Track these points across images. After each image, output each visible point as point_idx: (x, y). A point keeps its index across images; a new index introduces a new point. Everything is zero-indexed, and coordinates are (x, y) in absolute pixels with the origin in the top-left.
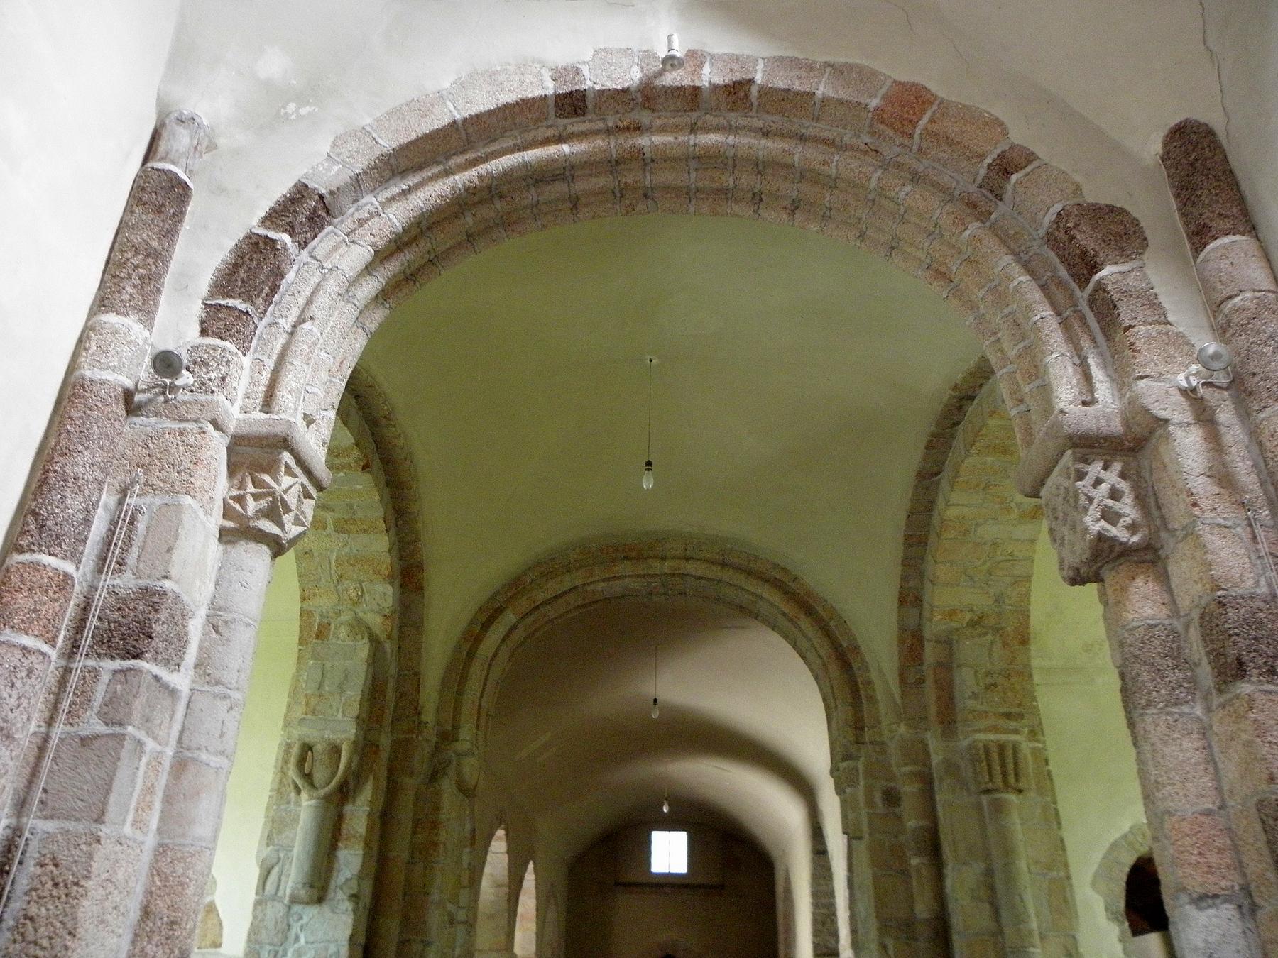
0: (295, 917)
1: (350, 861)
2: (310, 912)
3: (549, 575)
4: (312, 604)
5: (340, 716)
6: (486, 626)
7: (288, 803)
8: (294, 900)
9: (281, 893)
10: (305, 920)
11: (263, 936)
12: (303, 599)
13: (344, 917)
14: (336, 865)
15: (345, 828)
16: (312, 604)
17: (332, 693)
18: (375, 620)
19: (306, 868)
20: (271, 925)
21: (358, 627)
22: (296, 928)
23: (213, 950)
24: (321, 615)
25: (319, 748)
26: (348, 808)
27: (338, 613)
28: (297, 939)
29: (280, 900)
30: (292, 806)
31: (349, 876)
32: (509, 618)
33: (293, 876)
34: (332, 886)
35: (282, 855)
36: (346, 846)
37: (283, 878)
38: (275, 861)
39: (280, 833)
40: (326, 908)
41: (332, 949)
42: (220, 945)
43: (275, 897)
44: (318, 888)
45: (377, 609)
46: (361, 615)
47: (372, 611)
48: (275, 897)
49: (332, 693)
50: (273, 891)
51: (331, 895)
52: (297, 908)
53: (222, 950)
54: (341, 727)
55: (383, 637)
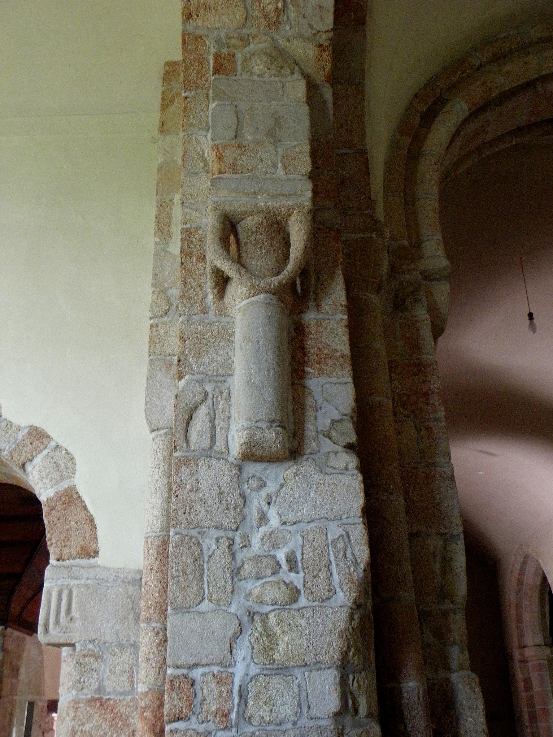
0: (254, 484)
1: (332, 395)
2: (279, 476)
3: (500, 58)
4: (197, 25)
5: (280, 172)
6: (429, 117)
7: (205, 311)
8: (252, 454)
9: (219, 446)
10: (271, 487)
11: (201, 515)
12: (188, 16)
13: (345, 479)
14: (309, 401)
15: (311, 344)
16: (197, 25)
17: (259, 143)
18: (306, 52)
19: (269, 395)
20: (212, 496)
21: (280, 58)
22: (257, 502)
23: (83, 562)
24: (218, 42)
25: (249, 222)
26: (310, 317)
27: (245, 41)
28: (263, 518)
29: (222, 456)
30: (212, 316)
31: (336, 415)
32: (458, 109)
33: (243, 410)
34: (310, 430)
35: (209, 388)
36: (321, 372)
37: (219, 425)
38: (199, 397)
39: (198, 354)
40: (307, 467)
41: (335, 531)
42: (96, 553)
43: (210, 451)
44: (289, 437)
45: (308, 33)
46: (281, 42)
47: (301, 36)
48: (210, 451)
49: (259, 143)
50: (206, 443)
51: (311, 445)
52: (252, 469)
53: (99, 561)
54: (284, 184)
55: (319, 78)
